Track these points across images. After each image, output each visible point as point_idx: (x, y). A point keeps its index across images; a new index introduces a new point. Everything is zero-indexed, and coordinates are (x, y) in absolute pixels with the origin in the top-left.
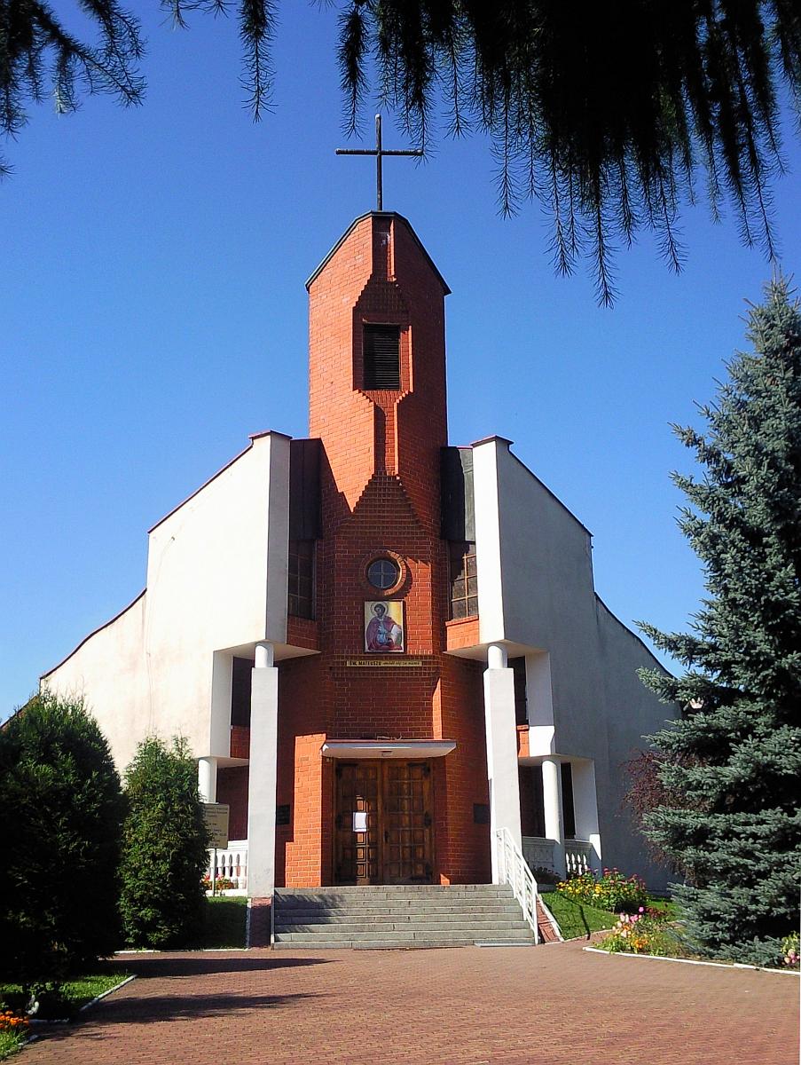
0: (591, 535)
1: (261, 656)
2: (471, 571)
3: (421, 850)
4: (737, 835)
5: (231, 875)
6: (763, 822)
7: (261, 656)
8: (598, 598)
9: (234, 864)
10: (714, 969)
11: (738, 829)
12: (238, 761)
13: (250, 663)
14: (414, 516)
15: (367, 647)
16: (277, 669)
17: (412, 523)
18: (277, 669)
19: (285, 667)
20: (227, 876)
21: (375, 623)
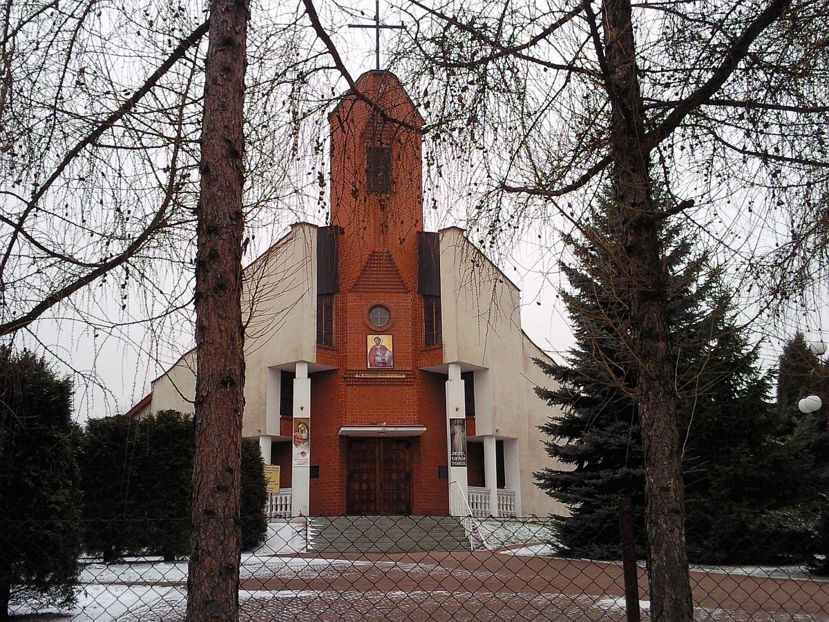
0: (519, 290)
1: (302, 374)
2: (439, 341)
3: (404, 495)
4: (586, 485)
5: (281, 510)
6: (599, 477)
7: (302, 374)
8: (523, 332)
9: (283, 502)
10: (313, 429)
11: (586, 481)
12: (285, 438)
13: (293, 375)
14: (400, 278)
15: (369, 365)
16: (310, 379)
17: (399, 282)
18: (310, 379)
19: (316, 377)
20: (479, 495)
21: (374, 349)
